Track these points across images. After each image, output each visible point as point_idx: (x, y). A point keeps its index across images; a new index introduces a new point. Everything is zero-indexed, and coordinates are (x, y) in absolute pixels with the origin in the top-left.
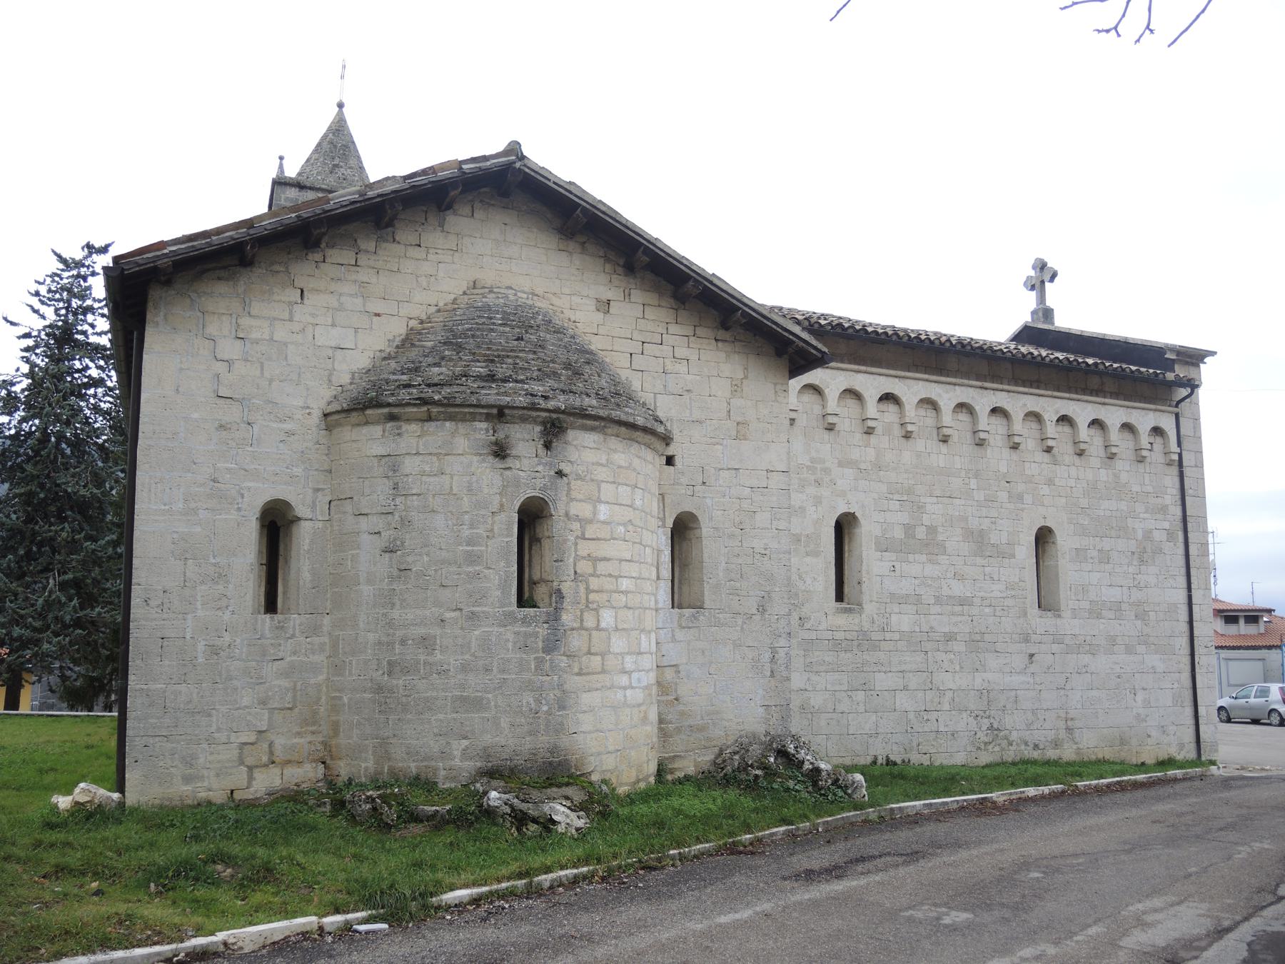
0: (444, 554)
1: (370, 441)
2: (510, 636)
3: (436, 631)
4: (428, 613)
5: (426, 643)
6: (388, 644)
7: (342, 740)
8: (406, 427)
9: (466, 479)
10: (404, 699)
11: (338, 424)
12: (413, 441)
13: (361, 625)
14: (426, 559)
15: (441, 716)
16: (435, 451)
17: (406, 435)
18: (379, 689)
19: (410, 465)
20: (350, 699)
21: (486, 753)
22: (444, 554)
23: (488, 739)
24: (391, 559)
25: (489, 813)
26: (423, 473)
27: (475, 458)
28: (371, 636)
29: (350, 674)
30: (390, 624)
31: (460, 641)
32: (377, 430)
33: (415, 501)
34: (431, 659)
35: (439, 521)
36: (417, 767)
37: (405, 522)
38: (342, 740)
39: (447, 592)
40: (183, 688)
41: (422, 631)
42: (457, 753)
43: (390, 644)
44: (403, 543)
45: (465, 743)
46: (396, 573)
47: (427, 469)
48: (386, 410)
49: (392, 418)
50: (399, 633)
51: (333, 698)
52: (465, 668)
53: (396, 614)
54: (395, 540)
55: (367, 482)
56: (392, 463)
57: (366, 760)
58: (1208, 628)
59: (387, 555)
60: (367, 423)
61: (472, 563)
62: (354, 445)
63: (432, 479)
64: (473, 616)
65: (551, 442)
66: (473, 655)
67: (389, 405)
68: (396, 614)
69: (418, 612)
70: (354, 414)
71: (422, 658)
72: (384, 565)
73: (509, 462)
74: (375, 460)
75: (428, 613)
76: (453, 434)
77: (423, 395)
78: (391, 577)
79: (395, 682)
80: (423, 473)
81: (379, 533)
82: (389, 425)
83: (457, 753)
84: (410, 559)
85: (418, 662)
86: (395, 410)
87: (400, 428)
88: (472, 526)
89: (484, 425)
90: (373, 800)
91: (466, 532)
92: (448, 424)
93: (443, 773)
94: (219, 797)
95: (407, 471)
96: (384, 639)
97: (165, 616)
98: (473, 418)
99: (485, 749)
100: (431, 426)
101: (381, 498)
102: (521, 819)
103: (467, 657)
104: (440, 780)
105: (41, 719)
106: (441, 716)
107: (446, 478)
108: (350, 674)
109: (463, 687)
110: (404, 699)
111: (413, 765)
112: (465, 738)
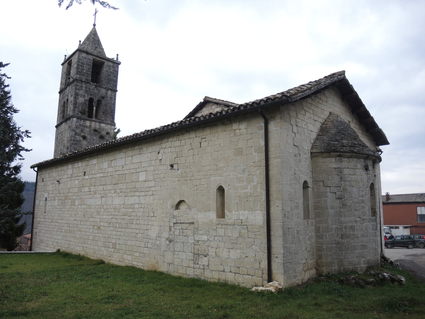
0: (356, 200)
1: (331, 163)
2: (371, 226)
3: (354, 224)
4: (352, 218)
5: (352, 228)
6: (341, 229)
7: (324, 260)
8: (343, 159)
9: (361, 177)
10: (347, 246)
11: (316, 156)
12: (346, 164)
13: (330, 223)
14: (351, 201)
15: (358, 251)
16: (353, 167)
17: (344, 162)
18: (338, 243)
19: (346, 171)
20: (326, 247)
21: (368, 262)
22: (356, 200)
23: (369, 258)
24: (340, 201)
25: (384, 279)
26: (350, 174)
27: (362, 170)
28: (334, 226)
29: (326, 238)
30: (341, 222)
31: (361, 227)
32: (333, 160)
33: (348, 183)
34: (354, 233)
35: (355, 190)
36: (352, 268)
37: (345, 190)
38: (324, 260)
39: (357, 212)
40: (293, 245)
41: (350, 224)
42: (362, 262)
43: (341, 229)
44: (344, 196)
45: (364, 259)
46: (341, 206)
47: (351, 173)
48: (339, 153)
49: (340, 156)
50: (344, 225)
51: (317, 247)
52: (362, 236)
53: (342, 219)
54: (341, 195)
55: (330, 176)
56: (340, 171)
57: (334, 266)
58: (381, 210)
59: (338, 200)
60: (329, 157)
61: (363, 203)
62: (324, 164)
63: (352, 176)
64: (363, 219)
65: (14, 110)
66: (364, 232)
67: (341, 152)
68: (342, 219)
69: (349, 218)
70: (326, 154)
71: (352, 233)
72: (337, 203)
73: (368, 171)
74: (333, 170)
75: (352, 218)
76: (357, 162)
77: (69, 102)
78: (340, 207)
79: (343, 241)
80: (350, 174)
81: (335, 193)
82: (337, 158)
83: (362, 262)
84: (347, 201)
85: (350, 234)
86: (342, 154)
87: (341, 159)
88: (362, 192)
89: (362, 160)
90: (355, 279)
91: (361, 193)
92: (355, 159)
93: (359, 269)
94: (300, 282)
95: (345, 173)
96: (339, 227)
97: (289, 220)
98: (361, 158)
99: (368, 260)
100: (351, 159)
101: (336, 181)
102: (393, 280)
103: (363, 232)
104: (358, 271)
105: (19, 255)
106: (358, 251)
107: (356, 176)
108: (326, 238)
109: (362, 242)
110: (347, 246)
111: (351, 267)
112: (364, 258)
